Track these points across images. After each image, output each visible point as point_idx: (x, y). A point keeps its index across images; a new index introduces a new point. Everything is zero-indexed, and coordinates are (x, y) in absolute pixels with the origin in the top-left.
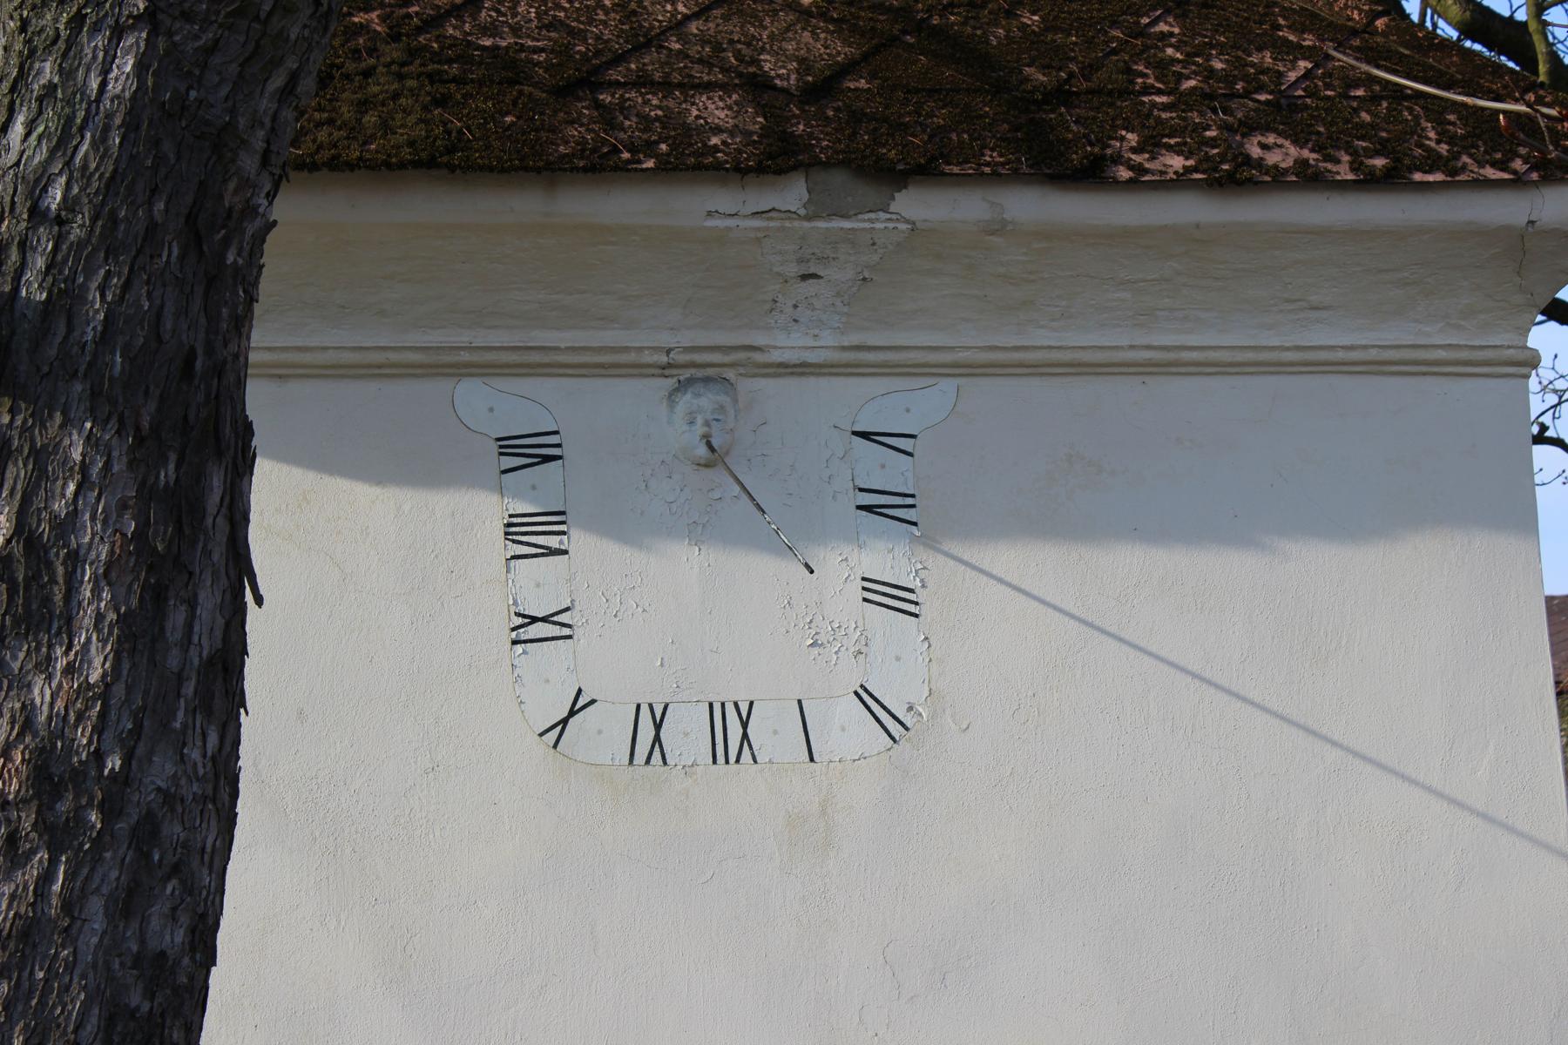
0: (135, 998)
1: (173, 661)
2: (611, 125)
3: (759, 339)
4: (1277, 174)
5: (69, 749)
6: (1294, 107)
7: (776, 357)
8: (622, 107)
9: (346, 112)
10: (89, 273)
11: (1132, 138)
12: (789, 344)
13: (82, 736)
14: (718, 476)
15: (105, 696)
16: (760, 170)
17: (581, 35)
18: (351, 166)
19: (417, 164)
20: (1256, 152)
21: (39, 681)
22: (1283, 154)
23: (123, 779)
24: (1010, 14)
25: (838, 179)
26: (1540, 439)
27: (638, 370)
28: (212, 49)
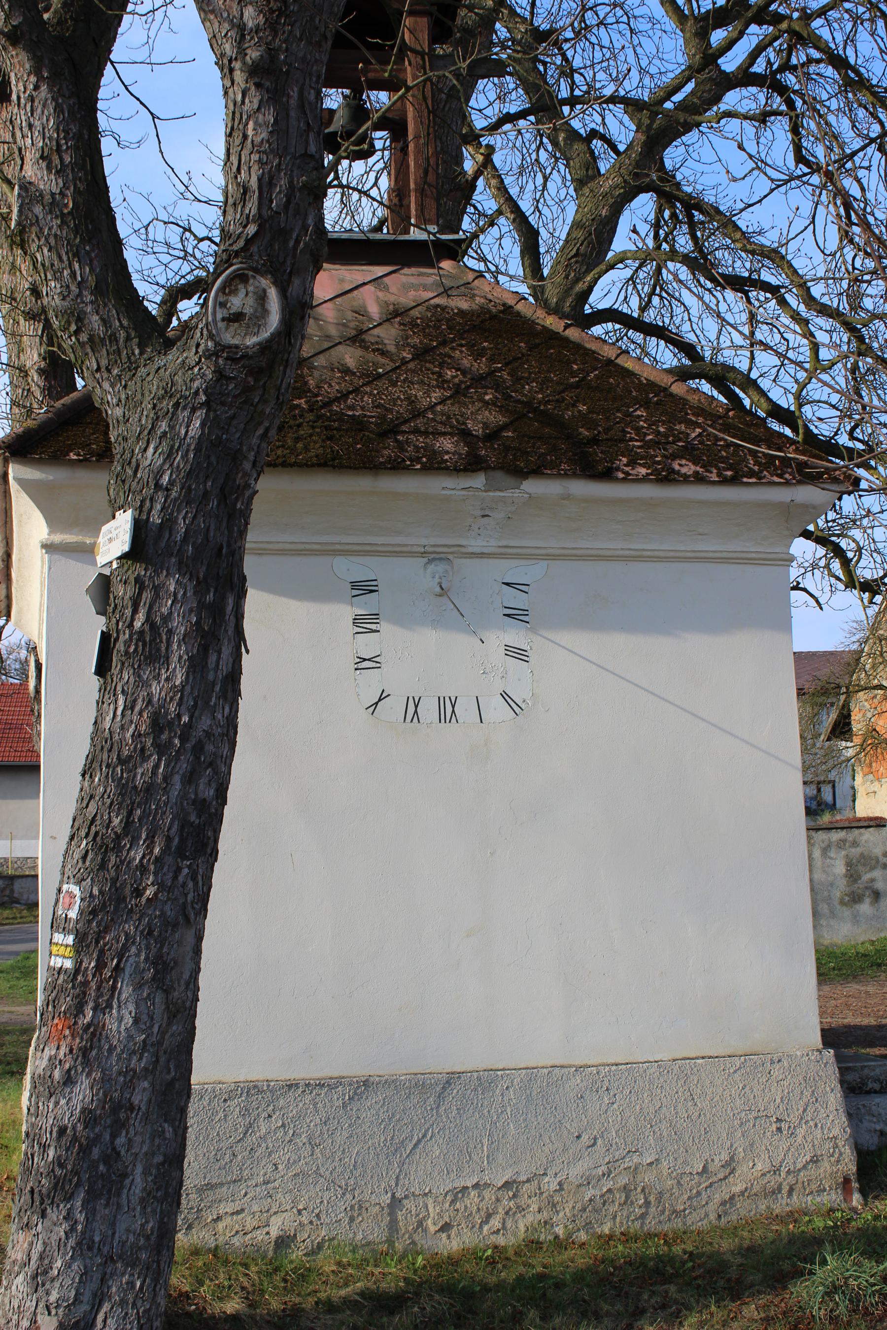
0: (193, 818)
1: (211, 677)
2: (402, 449)
5: (167, 713)
6: (694, 448)
7: (470, 550)
8: (407, 442)
9: (290, 442)
10: (179, 511)
11: (625, 460)
12: (476, 544)
13: (172, 707)
14: (444, 600)
15: (182, 691)
16: (465, 470)
17: (390, 411)
18: (291, 465)
19: (319, 465)
20: (677, 467)
21: (154, 684)
22: (689, 468)
23: (189, 726)
24: (574, 405)
25: (499, 475)
26: (796, 588)
27: (411, 554)
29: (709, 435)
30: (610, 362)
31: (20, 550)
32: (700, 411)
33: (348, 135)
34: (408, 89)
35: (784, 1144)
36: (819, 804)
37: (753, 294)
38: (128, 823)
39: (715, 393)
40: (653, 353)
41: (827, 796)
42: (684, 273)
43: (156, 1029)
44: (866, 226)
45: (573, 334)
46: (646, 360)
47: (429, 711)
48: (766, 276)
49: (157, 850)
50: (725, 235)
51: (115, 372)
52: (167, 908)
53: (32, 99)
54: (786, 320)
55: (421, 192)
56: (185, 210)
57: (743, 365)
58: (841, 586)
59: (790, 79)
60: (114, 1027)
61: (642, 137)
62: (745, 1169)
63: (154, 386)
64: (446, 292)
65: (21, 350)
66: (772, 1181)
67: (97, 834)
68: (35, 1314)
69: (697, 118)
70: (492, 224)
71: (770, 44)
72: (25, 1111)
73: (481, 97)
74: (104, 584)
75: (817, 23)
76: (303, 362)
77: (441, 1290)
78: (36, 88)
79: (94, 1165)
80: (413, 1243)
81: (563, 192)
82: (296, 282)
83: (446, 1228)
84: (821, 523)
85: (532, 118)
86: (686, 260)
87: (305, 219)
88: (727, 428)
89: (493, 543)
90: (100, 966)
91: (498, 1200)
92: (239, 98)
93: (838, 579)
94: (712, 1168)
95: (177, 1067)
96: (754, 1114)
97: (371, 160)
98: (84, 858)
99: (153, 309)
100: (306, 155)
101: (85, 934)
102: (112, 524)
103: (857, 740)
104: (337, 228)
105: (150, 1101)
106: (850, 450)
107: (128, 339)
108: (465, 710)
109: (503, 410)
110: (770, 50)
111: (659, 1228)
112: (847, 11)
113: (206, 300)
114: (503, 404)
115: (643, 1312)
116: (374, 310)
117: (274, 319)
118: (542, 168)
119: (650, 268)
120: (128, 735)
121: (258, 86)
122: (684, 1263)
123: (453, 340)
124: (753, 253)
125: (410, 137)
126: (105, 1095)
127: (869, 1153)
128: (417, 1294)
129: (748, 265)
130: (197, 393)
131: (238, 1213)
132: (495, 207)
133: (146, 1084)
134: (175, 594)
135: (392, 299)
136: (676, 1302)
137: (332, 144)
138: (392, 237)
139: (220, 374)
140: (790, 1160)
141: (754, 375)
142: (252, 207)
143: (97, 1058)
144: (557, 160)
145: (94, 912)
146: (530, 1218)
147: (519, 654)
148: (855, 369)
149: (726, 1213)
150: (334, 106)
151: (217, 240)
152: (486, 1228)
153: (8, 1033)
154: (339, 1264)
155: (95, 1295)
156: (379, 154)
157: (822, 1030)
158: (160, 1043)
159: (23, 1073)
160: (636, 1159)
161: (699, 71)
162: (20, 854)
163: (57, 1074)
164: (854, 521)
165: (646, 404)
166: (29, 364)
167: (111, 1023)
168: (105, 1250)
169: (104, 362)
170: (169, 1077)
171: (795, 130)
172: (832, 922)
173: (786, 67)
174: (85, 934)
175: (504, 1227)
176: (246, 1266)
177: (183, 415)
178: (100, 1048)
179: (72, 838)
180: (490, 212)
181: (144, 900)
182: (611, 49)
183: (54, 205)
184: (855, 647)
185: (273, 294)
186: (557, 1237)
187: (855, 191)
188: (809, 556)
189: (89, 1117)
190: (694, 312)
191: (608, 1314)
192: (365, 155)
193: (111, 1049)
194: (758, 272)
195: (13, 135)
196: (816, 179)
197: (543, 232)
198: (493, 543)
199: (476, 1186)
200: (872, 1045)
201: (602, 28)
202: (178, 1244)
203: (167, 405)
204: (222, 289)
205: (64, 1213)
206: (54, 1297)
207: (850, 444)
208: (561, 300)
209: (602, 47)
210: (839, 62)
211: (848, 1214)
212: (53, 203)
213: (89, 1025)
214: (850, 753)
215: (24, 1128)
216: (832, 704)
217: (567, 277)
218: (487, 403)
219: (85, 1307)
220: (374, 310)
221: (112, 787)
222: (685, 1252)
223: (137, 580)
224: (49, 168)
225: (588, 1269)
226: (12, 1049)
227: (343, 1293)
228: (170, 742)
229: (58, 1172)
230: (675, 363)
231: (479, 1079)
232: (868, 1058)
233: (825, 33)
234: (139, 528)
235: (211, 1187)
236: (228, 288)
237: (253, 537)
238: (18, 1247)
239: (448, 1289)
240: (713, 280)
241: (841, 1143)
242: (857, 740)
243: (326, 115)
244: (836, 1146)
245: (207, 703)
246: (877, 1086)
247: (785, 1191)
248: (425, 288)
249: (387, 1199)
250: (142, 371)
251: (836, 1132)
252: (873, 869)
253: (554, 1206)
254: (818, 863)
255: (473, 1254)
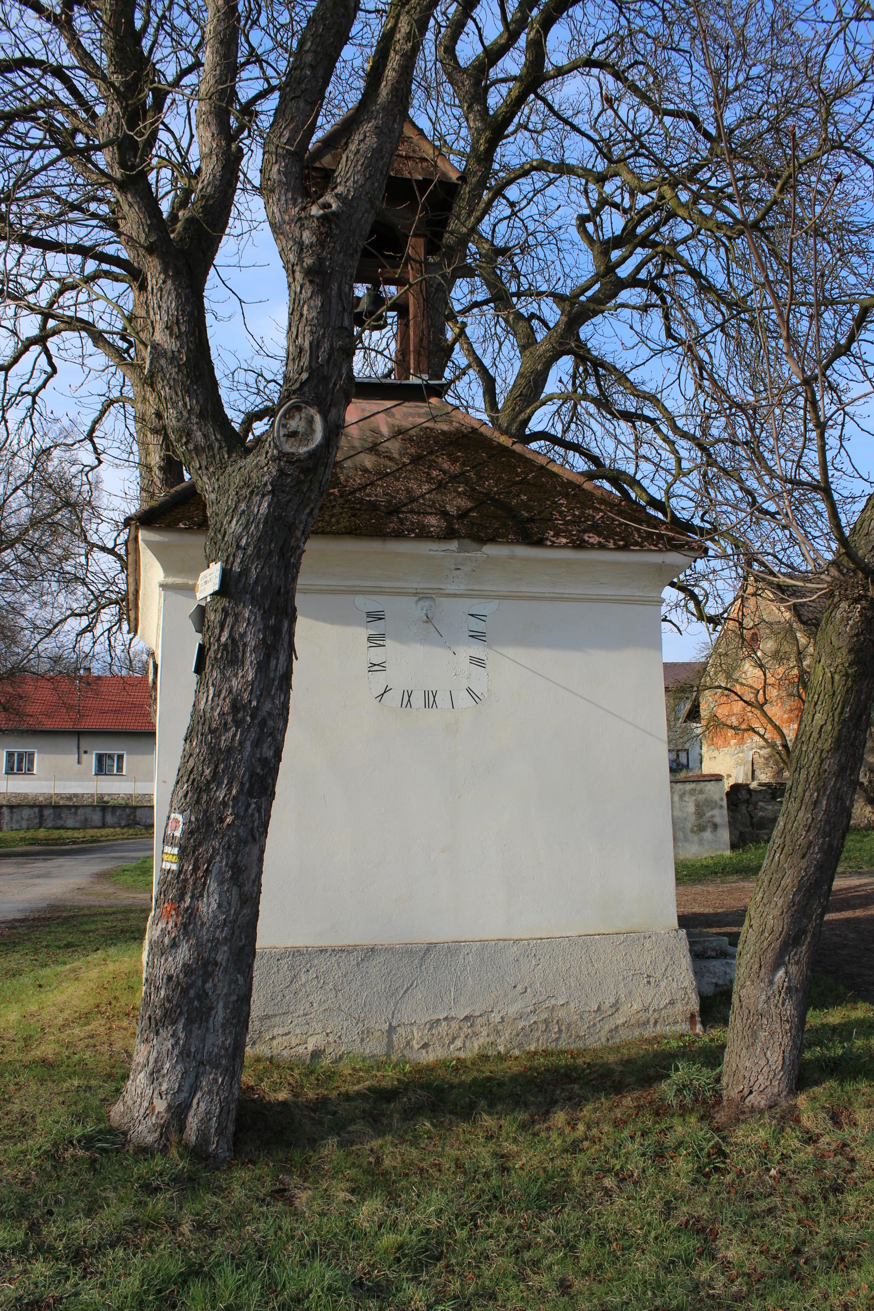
0: (259, 770)
1: (272, 675)
2: (402, 524)
3: (443, 587)
4: (592, 545)
5: (242, 699)
6: (598, 526)
7: (447, 592)
8: (406, 518)
9: (327, 518)
10: (252, 563)
11: (552, 533)
12: (451, 588)
13: (246, 696)
14: (429, 625)
15: (252, 685)
16: (445, 538)
17: (395, 498)
18: (328, 533)
19: (346, 533)
20: (587, 538)
21: (234, 679)
22: (595, 539)
23: (257, 708)
24: (518, 496)
25: (467, 542)
26: (665, 620)
27: (407, 594)
28: (290, 501)
29: (608, 517)
30: (542, 467)
31: (145, 588)
32: (602, 501)
33: (370, 314)
34: (411, 285)
35: (652, 992)
36: (678, 765)
37: (638, 423)
38: (215, 773)
39: (614, 491)
40: (571, 461)
41: (683, 759)
42: (592, 408)
43: (232, 912)
44: (714, 382)
45: (518, 448)
46: (567, 466)
47: (418, 699)
48: (647, 412)
49: (234, 792)
50: (620, 384)
51: (211, 469)
52: (241, 830)
53: (161, 289)
54: (659, 441)
55: (418, 354)
56: (259, 362)
57: (631, 470)
58: (695, 619)
59: (663, 283)
60: (205, 910)
61: (565, 319)
62: (625, 1008)
63: (237, 480)
64: (433, 418)
65: (148, 454)
66: (644, 1017)
67: (194, 780)
68: (152, 1098)
69: (602, 307)
70: (464, 374)
71: (650, 260)
72: (145, 964)
73: (458, 290)
74: (201, 612)
75: (681, 248)
76: (337, 464)
77: (422, 1087)
78: (164, 282)
79: (191, 1002)
80: (403, 1056)
81: (512, 353)
82: (334, 411)
83: (425, 1046)
84: (682, 577)
85: (492, 305)
86: (594, 400)
87: (340, 370)
88: (620, 513)
89: (462, 587)
90: (196, 869)
91: (460, 1028)
92: (298, 290)
93: (693, 614)
94: (603, 1008)
95: (247, 937)
96: (632, 972)
97: (384, 331)
98: (186, 796)
99: (236, 427)
100: (342, 328)
101: (186, 847)
102: (207, 571)
103: (704, 722)
104: (361, 375)
105: (228, 960)
106: (701, 529)
107: (220, 448)
108: (442, 699)
109: (470, 498)
110: (650, 264)
111: (568, 1047)
112: (700, 241)
113: (273, 422)
114: (471, 494)
115: (556, 1102)
116: (385, 430)
117: (319, 436)
118: (498, 338)
119: (569, 405)
120: (216, 714)
121: (311, 282)
122: (584, 1070)
123: (437, 451)
124: (638, 396)
125: (411, 317)
126: (198, 955)
127: (708, 998)
128: (406, 1090)
129: (635, 404)
130: (266, 484)
131: (286, 1034)
132: (466, 362)
133: (226, 948)
134: (249, 620)
135: (397, 423)
136: (578, 1095)
137: (359, 320)
138: (399, 382)
139: (281, 472)
140: (655, 1002)
141: (638, 477)
142: (305, 361)
143: (193, 930)
144: (508, 332)
145: (192, 833)
146: (481, 1040)
147: (479, 662)
148: (705, 475)
149: (612, 1037)
150: (360, 295)
151: (281, 382)
152: (452, 1047)
153: (132, 911)
154: (354, 1069)
155: (191, 1087)
156: (389, 327)
157: (678, 916)
158: (235, 921)
159: (142, 938)
160: (553, 1001)
161: (603, 277)
162: (140, 792)
163: (166, 940)
164: (704, 576)
165: (566, 496)
166: (153, 463)
167: (202, 907)
168: (199, 1057)
169: (204, 463)
170: (241, 944)
171: (666, 317)
172: (685, 844)
173: (660, 275)
174: (186, 847)
175: (464, 1046)
176: (292, 1069)
177: (256, 499)
178: (195, 924)
179: (177, 783)
180: (463, 366)
181: (225, 825)
182: (545, 261)
183: (173, 359)
184: (703, 660)
185: (318, 419)
186: (499, 1053)
187: (706, 358)
188: (674, 600)
189: (187, 969)
190: (599, 434)
191: (533, 1103)
192: (380, 328)
193: (203, 924)
194: (642, 410)
195: (148, 312)
196: (680, 350)
197: (499, 380)
198: (462, 587)
199: (446, 1019)
200: (711, 926)
201: (539, 248)
202: (247, 1054)
203: (246, 492)
204: (284, 416)
205: (171, 1032)
206: (164, 1087)
207: (701, 525)
208: (510, 425)
209: (539, 259)
210: (695, 274)
211: (693, 1038)
212: (173, 358)
213: (188, 908)
214: (699, 731)
215: (144, 976)
216: (687, 698)
217: (513, 409)
218: (459, 493)
219: (184, 1095)
220: (385, 430)
221: (205, 749)
222: (585, 1063)
223: (223, 609)
224: (171, 335)
225: (520, 1074)
226: (135, 923)
227: (356, 1088)
228: (244, 719)
229: (167, 1005)
230: (586, 468)
231: (449, 948)
232: (708, 935)
233: (686, 254)
234: (226, 575)
235: (268, 1017)
236: (288, 415)
237: (302, 581)
238: (140, 1054)
239: (427, 1086)
240: (611, 413)
241: (689, 992)
242: (704, 722)
243: (355, 301)
244: (686, 993)
245: (269, 693)
246: (714, 954)
247: (652, 1023)
248: (419, 416)
249: (386, 1027)
250: (229, 469)
251: (686, 984)
252: (713, 809)
253: (498, 1032)
254: (677, 805)
255: (443, 1064)
